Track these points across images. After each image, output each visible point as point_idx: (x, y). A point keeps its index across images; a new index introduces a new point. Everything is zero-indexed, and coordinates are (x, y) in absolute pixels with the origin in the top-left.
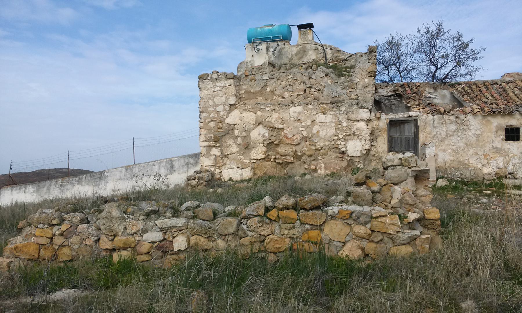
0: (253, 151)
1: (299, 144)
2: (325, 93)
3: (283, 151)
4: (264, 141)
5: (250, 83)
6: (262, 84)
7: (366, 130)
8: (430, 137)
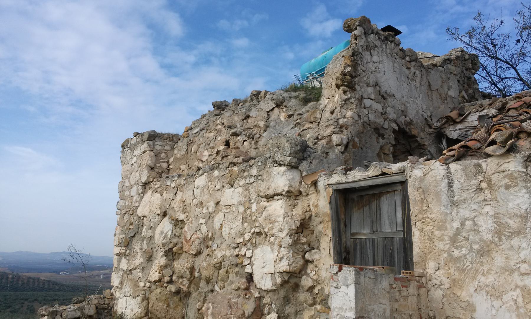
2: (262, 142)
8: (441, 239)
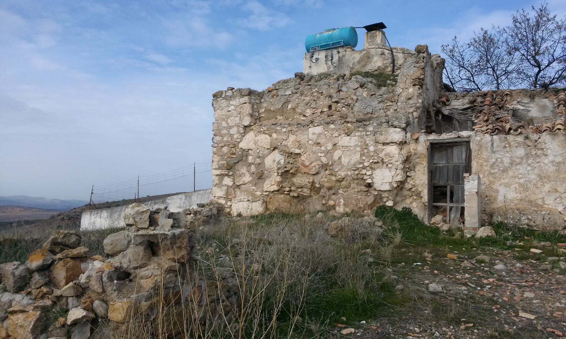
0: (266, 183)
1: (317, 173)
2: (356, 109)
3: (299, 181)
4: (279, 169)
5: (271, 100)
6: (283, 100)
7: (397, 155)
8: (486, 166)
